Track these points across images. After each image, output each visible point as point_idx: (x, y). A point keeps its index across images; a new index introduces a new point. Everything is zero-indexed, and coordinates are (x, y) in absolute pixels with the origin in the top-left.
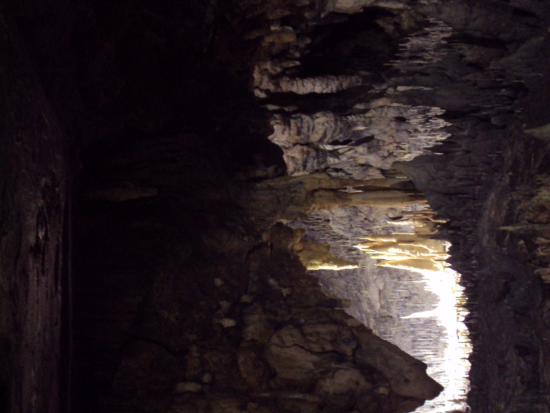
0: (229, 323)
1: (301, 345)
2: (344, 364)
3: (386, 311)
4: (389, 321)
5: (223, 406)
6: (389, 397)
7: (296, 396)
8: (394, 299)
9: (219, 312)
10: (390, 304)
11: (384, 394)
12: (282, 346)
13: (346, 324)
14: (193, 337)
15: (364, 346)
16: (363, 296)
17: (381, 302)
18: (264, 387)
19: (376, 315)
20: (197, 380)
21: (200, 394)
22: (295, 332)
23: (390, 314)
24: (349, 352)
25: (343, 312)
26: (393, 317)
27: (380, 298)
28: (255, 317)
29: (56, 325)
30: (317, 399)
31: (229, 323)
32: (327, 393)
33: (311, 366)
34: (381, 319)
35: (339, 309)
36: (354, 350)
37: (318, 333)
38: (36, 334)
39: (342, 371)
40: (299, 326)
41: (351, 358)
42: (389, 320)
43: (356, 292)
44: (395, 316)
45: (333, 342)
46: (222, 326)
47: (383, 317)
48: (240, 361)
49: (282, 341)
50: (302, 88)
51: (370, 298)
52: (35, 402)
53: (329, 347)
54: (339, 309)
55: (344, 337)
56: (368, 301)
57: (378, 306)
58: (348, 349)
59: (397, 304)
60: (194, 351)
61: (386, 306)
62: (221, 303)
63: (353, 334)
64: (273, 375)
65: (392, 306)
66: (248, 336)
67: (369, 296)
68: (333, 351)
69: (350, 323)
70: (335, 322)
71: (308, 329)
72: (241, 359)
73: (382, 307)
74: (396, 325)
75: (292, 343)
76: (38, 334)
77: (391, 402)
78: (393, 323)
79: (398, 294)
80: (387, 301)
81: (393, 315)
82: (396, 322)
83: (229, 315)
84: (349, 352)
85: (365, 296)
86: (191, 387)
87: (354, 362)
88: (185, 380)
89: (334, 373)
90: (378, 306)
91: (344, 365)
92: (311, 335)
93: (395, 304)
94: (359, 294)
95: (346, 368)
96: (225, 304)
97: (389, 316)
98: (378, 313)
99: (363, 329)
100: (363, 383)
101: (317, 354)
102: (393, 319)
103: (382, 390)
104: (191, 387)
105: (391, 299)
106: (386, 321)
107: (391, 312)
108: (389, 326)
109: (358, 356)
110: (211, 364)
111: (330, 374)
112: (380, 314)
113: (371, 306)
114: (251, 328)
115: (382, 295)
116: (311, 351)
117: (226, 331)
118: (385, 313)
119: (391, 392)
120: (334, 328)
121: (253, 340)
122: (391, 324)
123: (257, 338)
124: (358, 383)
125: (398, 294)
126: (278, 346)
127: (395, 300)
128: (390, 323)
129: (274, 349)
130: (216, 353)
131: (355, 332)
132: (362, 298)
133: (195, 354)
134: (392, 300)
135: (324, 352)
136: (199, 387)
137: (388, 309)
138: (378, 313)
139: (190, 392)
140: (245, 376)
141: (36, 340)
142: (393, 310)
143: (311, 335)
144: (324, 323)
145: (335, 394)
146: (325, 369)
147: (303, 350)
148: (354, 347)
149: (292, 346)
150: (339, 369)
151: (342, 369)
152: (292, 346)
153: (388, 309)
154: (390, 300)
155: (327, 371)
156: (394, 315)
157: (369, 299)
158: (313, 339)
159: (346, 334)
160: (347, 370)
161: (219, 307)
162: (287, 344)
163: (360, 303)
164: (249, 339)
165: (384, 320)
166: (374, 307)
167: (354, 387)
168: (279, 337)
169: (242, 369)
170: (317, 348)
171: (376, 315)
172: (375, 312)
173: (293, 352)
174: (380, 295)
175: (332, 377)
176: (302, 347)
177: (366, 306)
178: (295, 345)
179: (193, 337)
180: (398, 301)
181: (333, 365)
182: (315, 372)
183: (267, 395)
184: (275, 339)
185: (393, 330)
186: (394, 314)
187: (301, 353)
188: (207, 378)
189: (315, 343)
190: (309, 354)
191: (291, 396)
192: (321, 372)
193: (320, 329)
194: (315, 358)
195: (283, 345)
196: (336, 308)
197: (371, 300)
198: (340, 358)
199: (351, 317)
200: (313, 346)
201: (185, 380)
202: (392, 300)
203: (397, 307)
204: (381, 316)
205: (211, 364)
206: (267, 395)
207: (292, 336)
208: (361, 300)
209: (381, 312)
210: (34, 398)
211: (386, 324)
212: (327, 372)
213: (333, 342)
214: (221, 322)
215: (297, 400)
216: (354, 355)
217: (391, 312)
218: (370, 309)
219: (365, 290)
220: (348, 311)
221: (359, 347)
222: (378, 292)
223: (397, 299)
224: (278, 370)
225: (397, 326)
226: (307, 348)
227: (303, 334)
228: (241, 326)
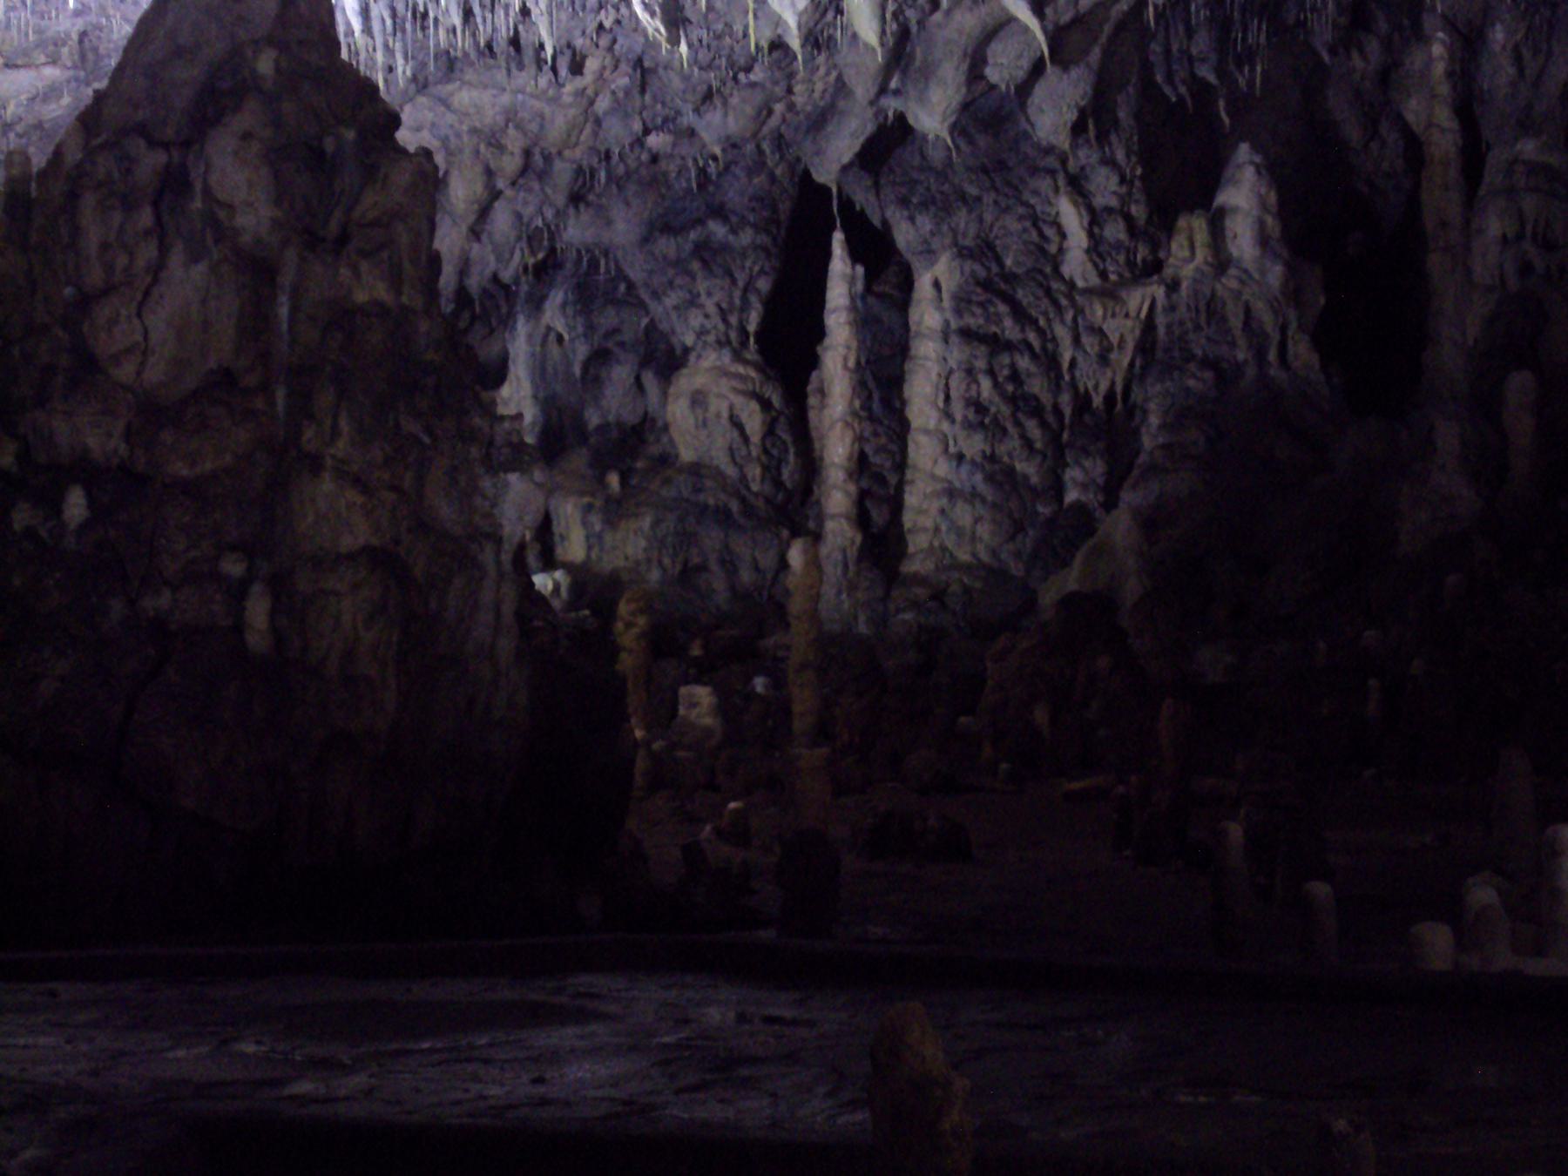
0: (76, 505)
1: (139, 296)
2: (193, 175)
3: (65, 50)
4: (94, 40)
5: (310, 519)
6: (282, 46)
7: (284, 311)
8: (27, 24)
9: (43, 533)
10: (44, 36)
11: (277, 62)
12: (144, 353)
13: (78, 166)
14: (117, 607)
15: (140, 115)
16: (23, 115)
17: (38, 62)
18: (259, 403)
19: (77, 79)
20: (238, 593)
21: (279, 586)
22: (103, 312)
23: (75, 37)
24: (160, 158)
25: (43, 174)
26: (82, 29)
27: (26, 66)
28: (61, 427)
29: (53, 994)
30: (291, 255)
31: (76, 505)
32: (276, 223)
33: (201, 268)
34: (90, 65)
35: (34, 185)
36: (153, 143)
37: (105, 246)
38: (68, 1047)
39: (214, 179)
40: (86, 302)
41: (176, 156)
42: (90, 41)
43: (12, 136)
44: (80, 24)
45: (129, 205)
46: (85, 526)
47: (83, 57)
48: (185, 472)
49: (129, 351)
50: (1156, 295)
51: (30, 96)
52: (258, 1043)
53: (146, 217)
54: (34, 185)
55: (116, 175)
56: (38, 99)
57: (51, 72)
58: (150, 162)
59: (43, 18)
60: (158, 602)
61: (51, 48)
62: (17, 527)
63: (102, 147)
64: (226, 378)
65: (50, 33)
66: (116, 450)
67: (23, 97)
68: (156, 205)
69: (73, 156)
70: (73, 196)
71: (95, 277)
72: (181, 469)
73: (54, 61)
74: (104, 21)
75: (136, 321)
76: (68, 1042)
77: (300, 42)
78: (101, 29)
79: (12, 14)
80: (37, 46)
81: (76, 29)
82: (95, 21)
83: (53, 504)
84: (160, 158)
85: (21, 109)
86: (258, 610)
87: (186, 144)
88: (238, 629)
89: (221, 204)
90: (51, 72)
91: (196, 174)
92: (109, 268)
93: (44, 23)
94: (19, 128)
95: (203, 169)
96: (22, 517)
97: (81, 41)
98: (71, 73)
99: (89, 119)
100: (247, 118)
101: (163, 250)
102: (89, 28)
103: (265, 64)
104: (258, 610)
105: (27, 35)
106: (95, 50)
107: (68, 35)
108: (109, 41)
109: (170, 133)
110: (193, 554)
111: (222, 214)
112: (75, 67)
113: (50, 93)
114: (93, 441)
115: (19, 62)
116: (157, 269)
117: (98, 512)
118: (71, 54)
119: (271, 41)
120: (89, 201)
121: (128, 435)
122: (102, 35)
123: (120, 425)
124: (247, 136)
125: (12, 14)
126: (142, 364)
127: (31, 23)
128: (99, 38)
129: (155, 373)
130: (163, 541)
131: (99, 140)
132: (31, 120)
133: (164, 600)
134: (31, 32)
135: (159, 231)
136: (256, 588)
137: (58, 42)
138: (71, 73)
139: (273, 614)
140: (228, 458)
141: (84, 1047)
142: (61, 29)
143: (109, 268)
144: (76, 231)
145: (278, 202)
146: (208, 230)
147: (155, 292)
148: (142, 143)
149: (142, 322)
150: (207, 192)
151: (205, 181)
152: (142, 322)
153: (60, 43)
154: (31, 38)
155: (213, 222)
156: (75, 27)
157: (32, 99)
158: (122, 261)
159: (105, 165)
160: (208, 166)
161: (30, 533)
162: (139, 338)
163: (47, 126)
164: (123, 447)
165: (90, 56)
166: (53, 83)
167: (255, 147)
168: (117, 359)
169: (208, 466)
170: (147, 252)
171: (77, 79)
172: (69, 81)
173: (158, 321)
174: (16, 66)
175: (230, 207)
176: (147, 294)
177: (53, 106)
178: (139, 315)
179: (117, 607)
180: (33, 12)
181: (198, 204)
182: (215, 257)
183: (280, 394)
184: (125, 372)
185: (119, 31)
186: (73, 25)
187: (161, 297)
188: (234, 567)
189: (131, 255)
190: (164, 275)
191: (285, 327)
192: (217, 241)
193: (93, 237)
194: (176, 258)
195: (144, 350)
196: (34, 194)
197: (34, 91)
198: (174, 184)
199: (58, 153)
200: (141, 263)
201: (239, 629)
202: (31, 32)
203: (50, 19)
204: (79, 64)
205: (193, 554)
206: (280, 394)
207: (113, 321)
208: (36, 122)
209: (69, 64)
210: (249, 1048)
211: (102, 51)
212: (217, 226)
213: (129, 205)
214: (72, 526)
215: (294, 309)
216: (166, 146)
217: (68, 35)
218: (60, 97)
219: (5, 108)
220: (39, 160)
221: (142, 130)
222: (9, 71)
223: (25, 16)
224: (213, 364)
225: (108, 18)
226: (149, 279)
227: (108, 290)
228: (85, 471)
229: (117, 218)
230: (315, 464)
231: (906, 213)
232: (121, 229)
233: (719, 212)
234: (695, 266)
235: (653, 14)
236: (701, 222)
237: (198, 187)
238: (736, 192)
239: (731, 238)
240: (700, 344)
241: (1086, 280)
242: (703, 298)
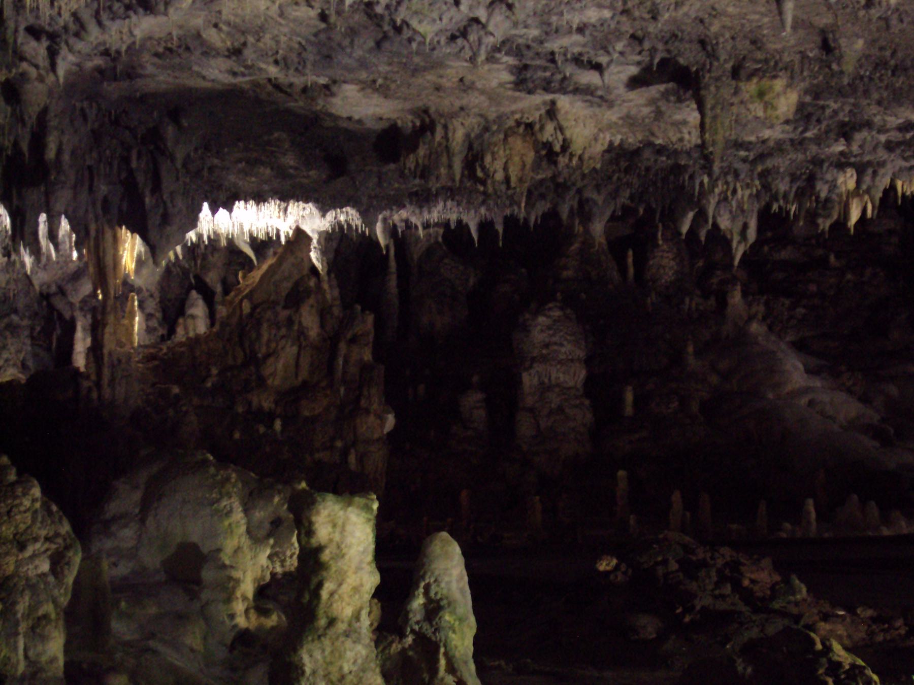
0: (278, 425)
31: (278, 425)
39: (303, 319)
83: (270, 426)
124: (312, 306)
193: (265, 336)
212: (302, 333)
229: (274, 332)
230: (367, 412)
231: (83, 314)
232: (275, 335)
233: (15, 311)
234: (8, 333)
235: (319, 262)
236: (7, 315)
237: (297, 322)
238: (21, 304)
239: (20, 321)
240: (6, 365)
241: (144, 342)
242: (9, 346)
